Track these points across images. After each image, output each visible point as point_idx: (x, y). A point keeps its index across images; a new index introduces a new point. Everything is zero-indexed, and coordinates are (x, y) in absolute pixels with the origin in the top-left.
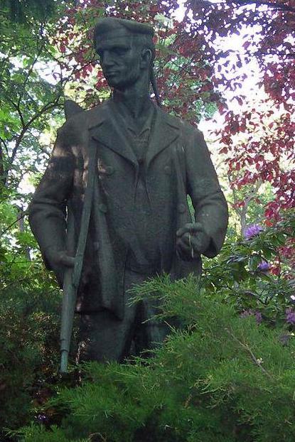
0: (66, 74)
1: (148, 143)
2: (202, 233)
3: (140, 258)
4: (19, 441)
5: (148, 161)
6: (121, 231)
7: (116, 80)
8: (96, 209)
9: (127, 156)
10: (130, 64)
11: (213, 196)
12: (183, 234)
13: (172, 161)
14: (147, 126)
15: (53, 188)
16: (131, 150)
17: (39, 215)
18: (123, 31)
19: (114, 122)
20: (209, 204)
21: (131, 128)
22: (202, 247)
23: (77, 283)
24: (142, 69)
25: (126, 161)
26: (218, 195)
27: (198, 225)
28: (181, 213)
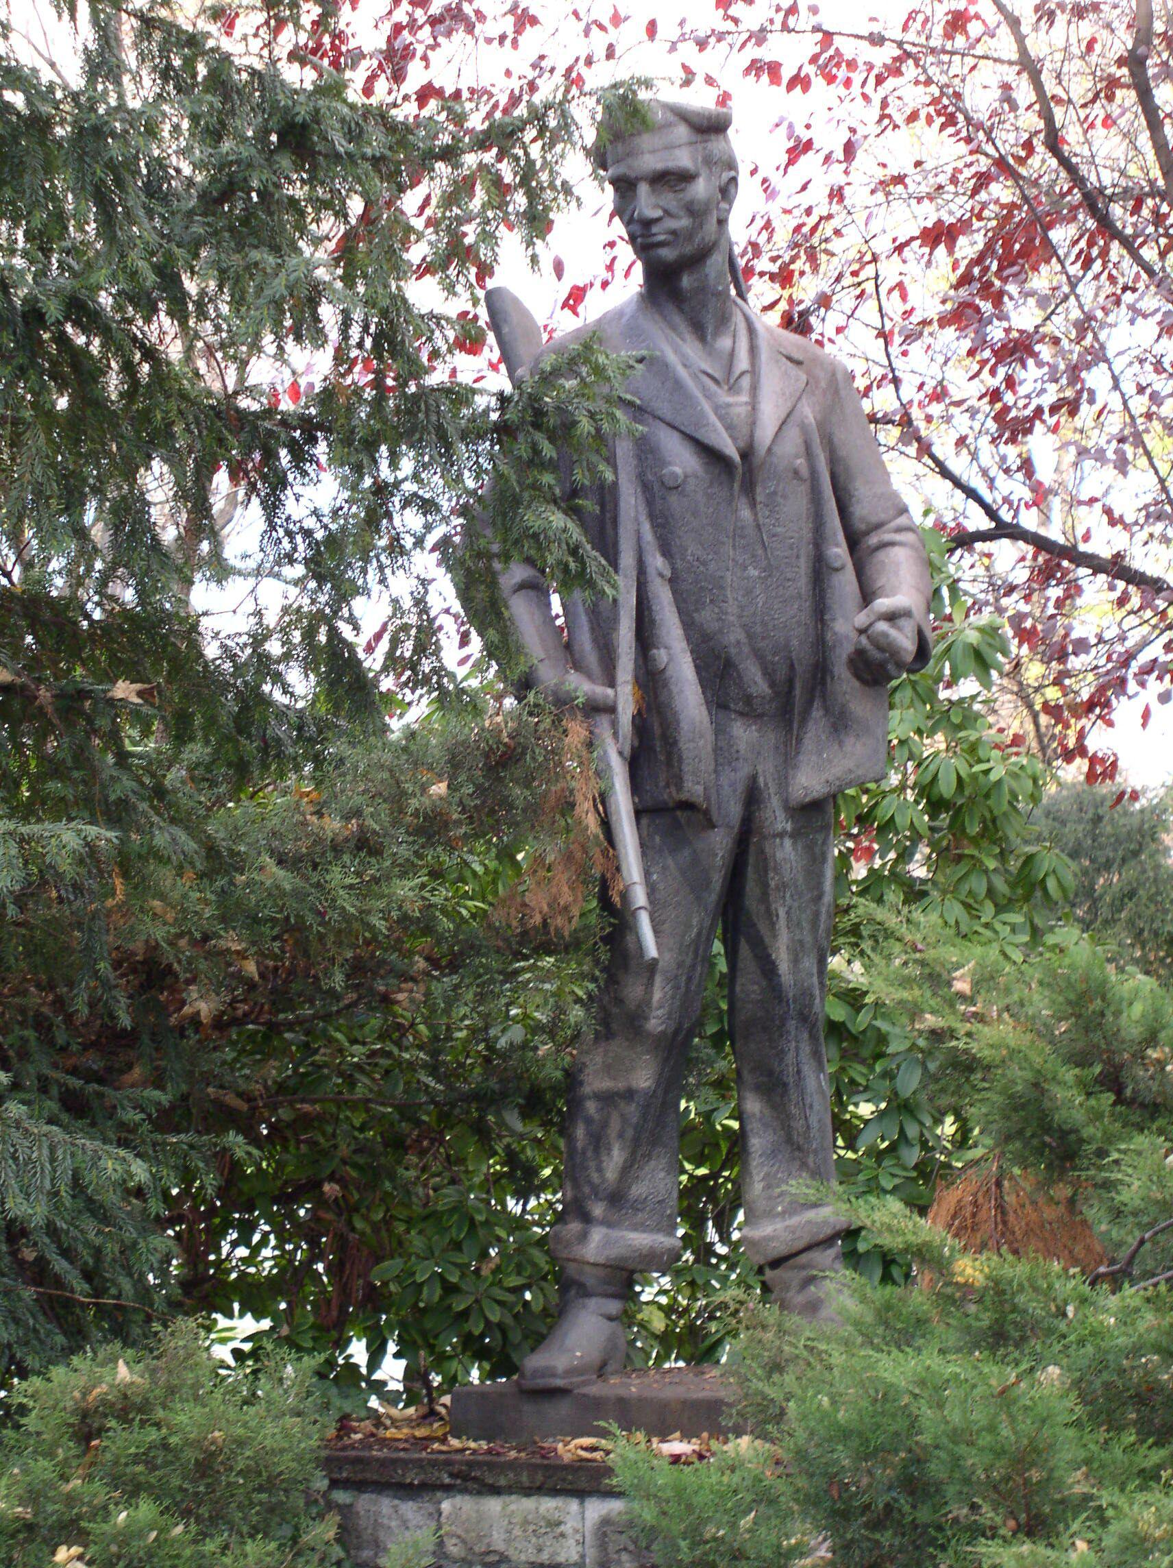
1: (754, 405)
6: (706, 616)
12: (871, 625)
14: (743, 363)
16: (719, 425)
18: (682, 132)
20: (892, 544)
21: (710, 371)
23: (627, 751)
25: (710, 454)
28: (837, 570)
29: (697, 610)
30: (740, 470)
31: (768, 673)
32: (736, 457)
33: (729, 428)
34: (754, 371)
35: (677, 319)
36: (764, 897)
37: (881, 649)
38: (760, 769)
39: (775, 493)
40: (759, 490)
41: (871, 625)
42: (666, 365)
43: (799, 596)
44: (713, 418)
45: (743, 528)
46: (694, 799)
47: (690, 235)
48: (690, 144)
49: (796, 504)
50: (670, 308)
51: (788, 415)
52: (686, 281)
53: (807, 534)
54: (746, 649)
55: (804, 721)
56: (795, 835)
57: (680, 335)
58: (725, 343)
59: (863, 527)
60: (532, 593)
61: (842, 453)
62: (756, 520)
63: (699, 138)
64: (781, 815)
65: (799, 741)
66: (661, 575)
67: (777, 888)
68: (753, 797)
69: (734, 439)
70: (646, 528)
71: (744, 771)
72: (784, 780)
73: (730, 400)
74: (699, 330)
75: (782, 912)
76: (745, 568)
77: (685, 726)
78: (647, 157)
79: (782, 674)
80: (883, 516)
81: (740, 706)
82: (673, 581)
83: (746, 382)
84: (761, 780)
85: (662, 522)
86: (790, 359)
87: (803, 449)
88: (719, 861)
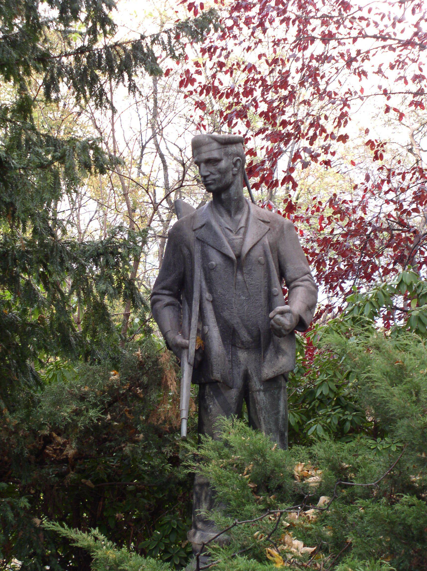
1: (244, 239)
2: (290, 314)
3: (244, 335)
5: (244, 254)
6: (226, 314)
7: (213, 187)
8: (204, 298)
9: (226, 252)
10: (223, 172)
11: (301, 279)
12: (274, 316)
13: (265, 252)
14: (242, 224)
15: (170, 280)
16: (229, 246)
17: (158, 305)
18: (215, 145)
19: (214, 223)
20: (299, 286)
21: (229, 227)
22: (290, 325)
23: (192, 361)
24: (234, 175)
25: (226, 257)
26: (306, 277)
27: (287, 307)
28: (275, 296)
29: (222, 312)
30: (236, 262)
31: (250, 333)
32: (234, 257)
33: (233, 247)
34: (246, 227)
35: (222, 209)
36: (256, 412)
37: (279, 325)
38: (249, 367)
39: (251, 269)
40: (244, 268)
41: (274, 316)
42: (212, 226)
43: (261, 305)
44: (227, 244)
45: (239, 282)
46: (217, 379)
47: (220, 180)
50: (219, 205)
51: (258, 242)
52: (223, 196)
53: (264, 282)
54: (241, 325)
55: (266, 350)
56: (265, 391)
57: (222, 216)
58: (239, 217)
59: (290, 280)
60: (171, 307)
61: (282, 254)
62: (244, 279)
63: (222, 147)
64: (258, 384)
65: (264, 357)
66: (208, 300)
67: (259, 410)
68: (246, 378)
69: (234, 251)
70: (204, 283)
71: (243, 368)
72: (259, 371)
73: (234, 237)
74: (229, 212)
75: (262, 418)
76: (240, 296)
77: (213, 353)
78: (203, 154)
79: (255, 334)
80: (297, 276)
81: (240, 345)
82: (213, 302)
83: (242, 231)
84: (249, 371)
86: (263, 221)
87: (263, 253)
88: (234, 401)
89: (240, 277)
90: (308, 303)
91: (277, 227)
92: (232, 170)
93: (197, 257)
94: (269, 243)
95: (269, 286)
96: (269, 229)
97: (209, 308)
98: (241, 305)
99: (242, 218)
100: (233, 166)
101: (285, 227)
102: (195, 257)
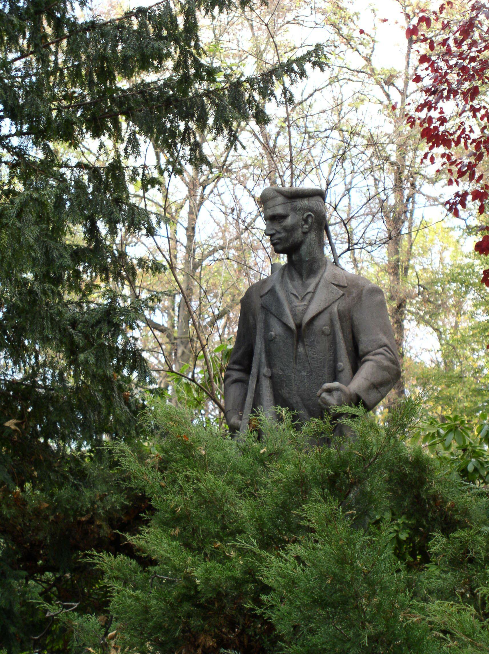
0: (408, 101)
1: (308, 306)
2: (339, 392)
4: (3, 353)
5: (304, 324)
8: (261, 374)
9: (285, 320)
13: (332, 321)
14: (311, 289)
18: (280, 199)
21: (295, 293)
24: (305, 233)
25: (286, 326)
32: (292, 325)
33: (294, 315)
34: (314, 293)
39: (314, 341)
42: (275, 292)
45: (300, 356)
47: (286, 239)
48: (284, 203)
49: (323, 344)
51: (325, 309)
60: (240, 384)
61: (356, 323)
62: (305, 352)
66: (265, 376)
70: (263, 356)
73: (297, 304)
74: (301, 275)
76: (300, 372)
80: (370, 349)
85: (269, 354)
89: (301, 350)
90: (373, 380)
91: (355, 291)
92: (302, 228)
93: (260, 326)
94: (338, 311)
95: (335, 359)
96: (343, 295)
97: (266, 384)
98: (302, 382)
99: (313, 282)
100: (303, 223)
101: (364, 292)
102: (258, 327)
